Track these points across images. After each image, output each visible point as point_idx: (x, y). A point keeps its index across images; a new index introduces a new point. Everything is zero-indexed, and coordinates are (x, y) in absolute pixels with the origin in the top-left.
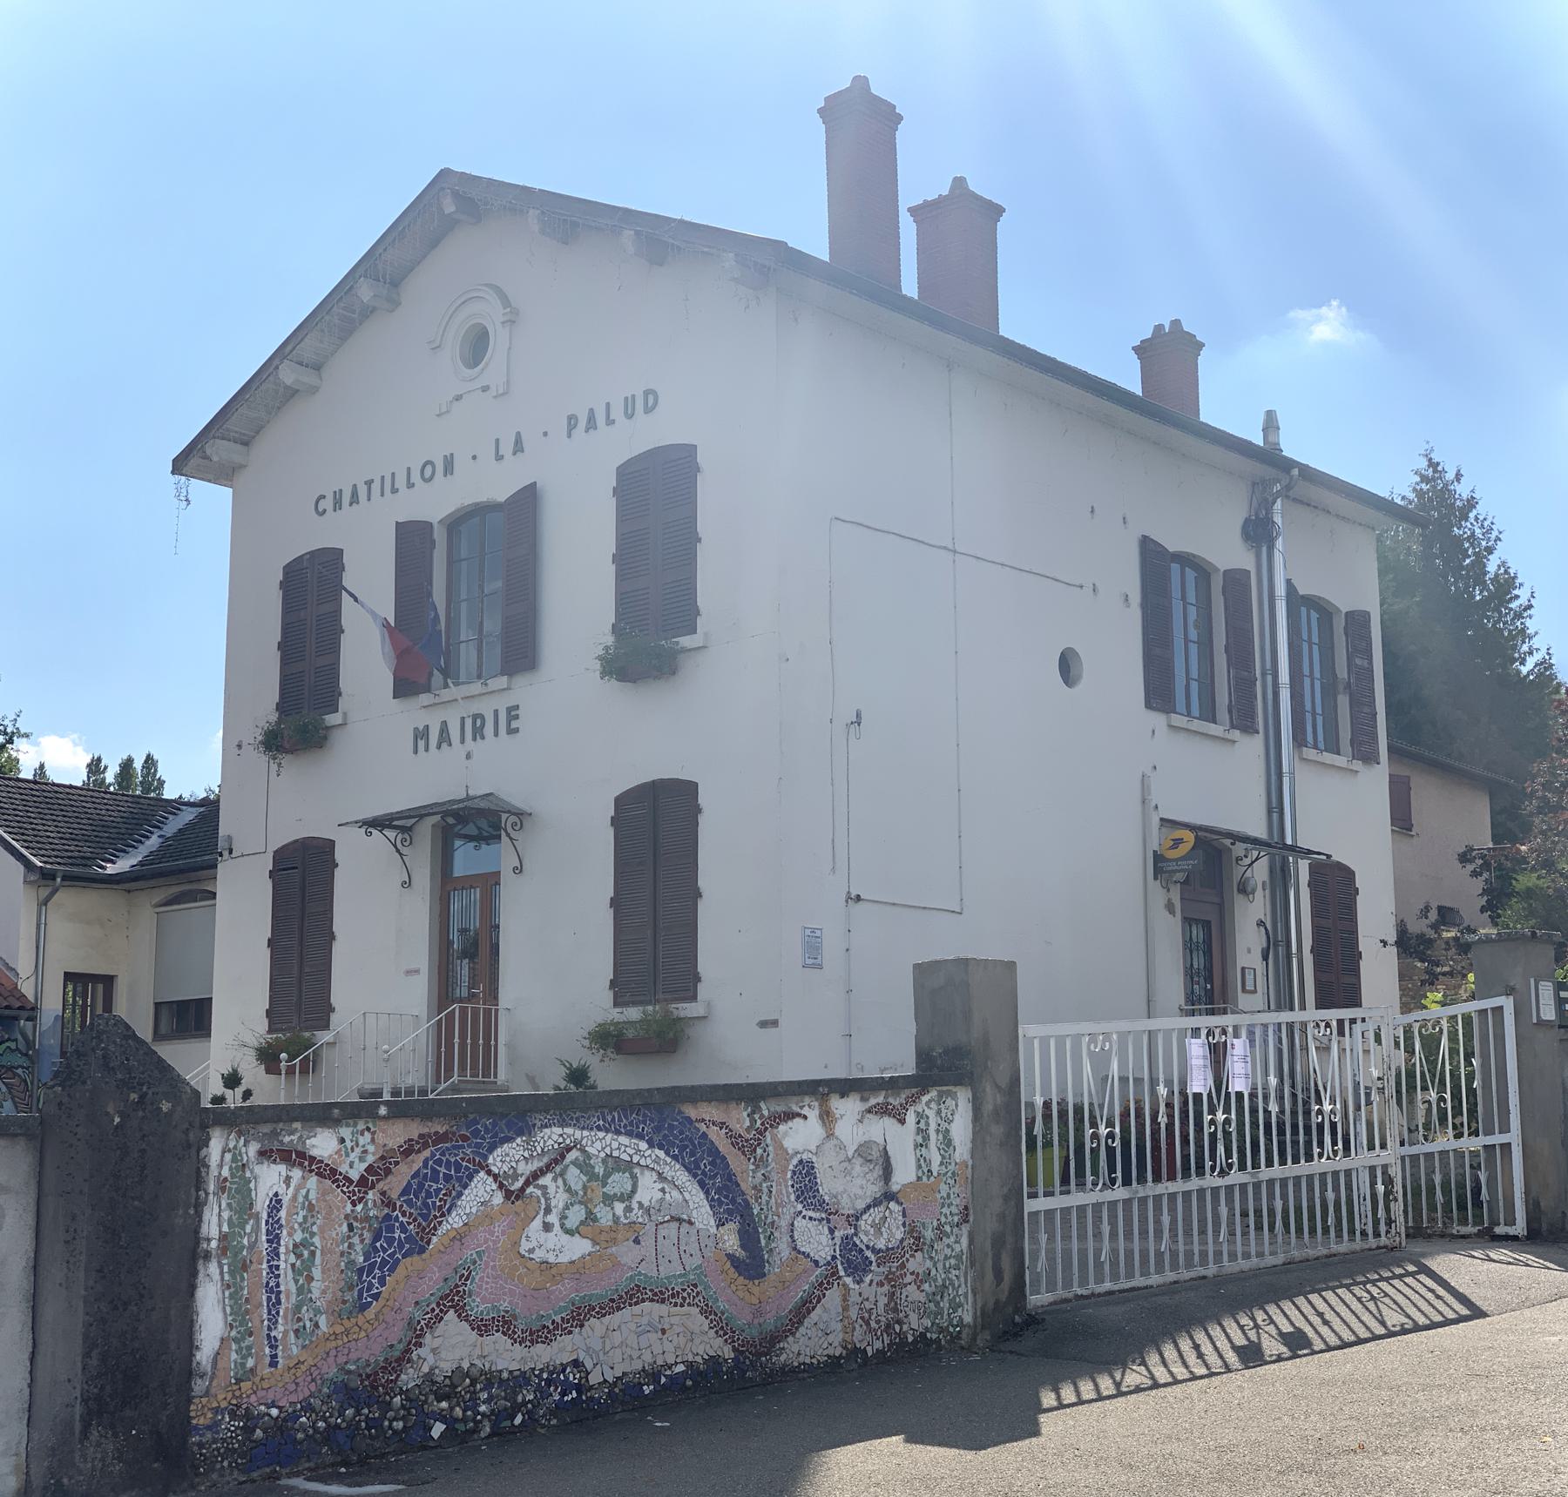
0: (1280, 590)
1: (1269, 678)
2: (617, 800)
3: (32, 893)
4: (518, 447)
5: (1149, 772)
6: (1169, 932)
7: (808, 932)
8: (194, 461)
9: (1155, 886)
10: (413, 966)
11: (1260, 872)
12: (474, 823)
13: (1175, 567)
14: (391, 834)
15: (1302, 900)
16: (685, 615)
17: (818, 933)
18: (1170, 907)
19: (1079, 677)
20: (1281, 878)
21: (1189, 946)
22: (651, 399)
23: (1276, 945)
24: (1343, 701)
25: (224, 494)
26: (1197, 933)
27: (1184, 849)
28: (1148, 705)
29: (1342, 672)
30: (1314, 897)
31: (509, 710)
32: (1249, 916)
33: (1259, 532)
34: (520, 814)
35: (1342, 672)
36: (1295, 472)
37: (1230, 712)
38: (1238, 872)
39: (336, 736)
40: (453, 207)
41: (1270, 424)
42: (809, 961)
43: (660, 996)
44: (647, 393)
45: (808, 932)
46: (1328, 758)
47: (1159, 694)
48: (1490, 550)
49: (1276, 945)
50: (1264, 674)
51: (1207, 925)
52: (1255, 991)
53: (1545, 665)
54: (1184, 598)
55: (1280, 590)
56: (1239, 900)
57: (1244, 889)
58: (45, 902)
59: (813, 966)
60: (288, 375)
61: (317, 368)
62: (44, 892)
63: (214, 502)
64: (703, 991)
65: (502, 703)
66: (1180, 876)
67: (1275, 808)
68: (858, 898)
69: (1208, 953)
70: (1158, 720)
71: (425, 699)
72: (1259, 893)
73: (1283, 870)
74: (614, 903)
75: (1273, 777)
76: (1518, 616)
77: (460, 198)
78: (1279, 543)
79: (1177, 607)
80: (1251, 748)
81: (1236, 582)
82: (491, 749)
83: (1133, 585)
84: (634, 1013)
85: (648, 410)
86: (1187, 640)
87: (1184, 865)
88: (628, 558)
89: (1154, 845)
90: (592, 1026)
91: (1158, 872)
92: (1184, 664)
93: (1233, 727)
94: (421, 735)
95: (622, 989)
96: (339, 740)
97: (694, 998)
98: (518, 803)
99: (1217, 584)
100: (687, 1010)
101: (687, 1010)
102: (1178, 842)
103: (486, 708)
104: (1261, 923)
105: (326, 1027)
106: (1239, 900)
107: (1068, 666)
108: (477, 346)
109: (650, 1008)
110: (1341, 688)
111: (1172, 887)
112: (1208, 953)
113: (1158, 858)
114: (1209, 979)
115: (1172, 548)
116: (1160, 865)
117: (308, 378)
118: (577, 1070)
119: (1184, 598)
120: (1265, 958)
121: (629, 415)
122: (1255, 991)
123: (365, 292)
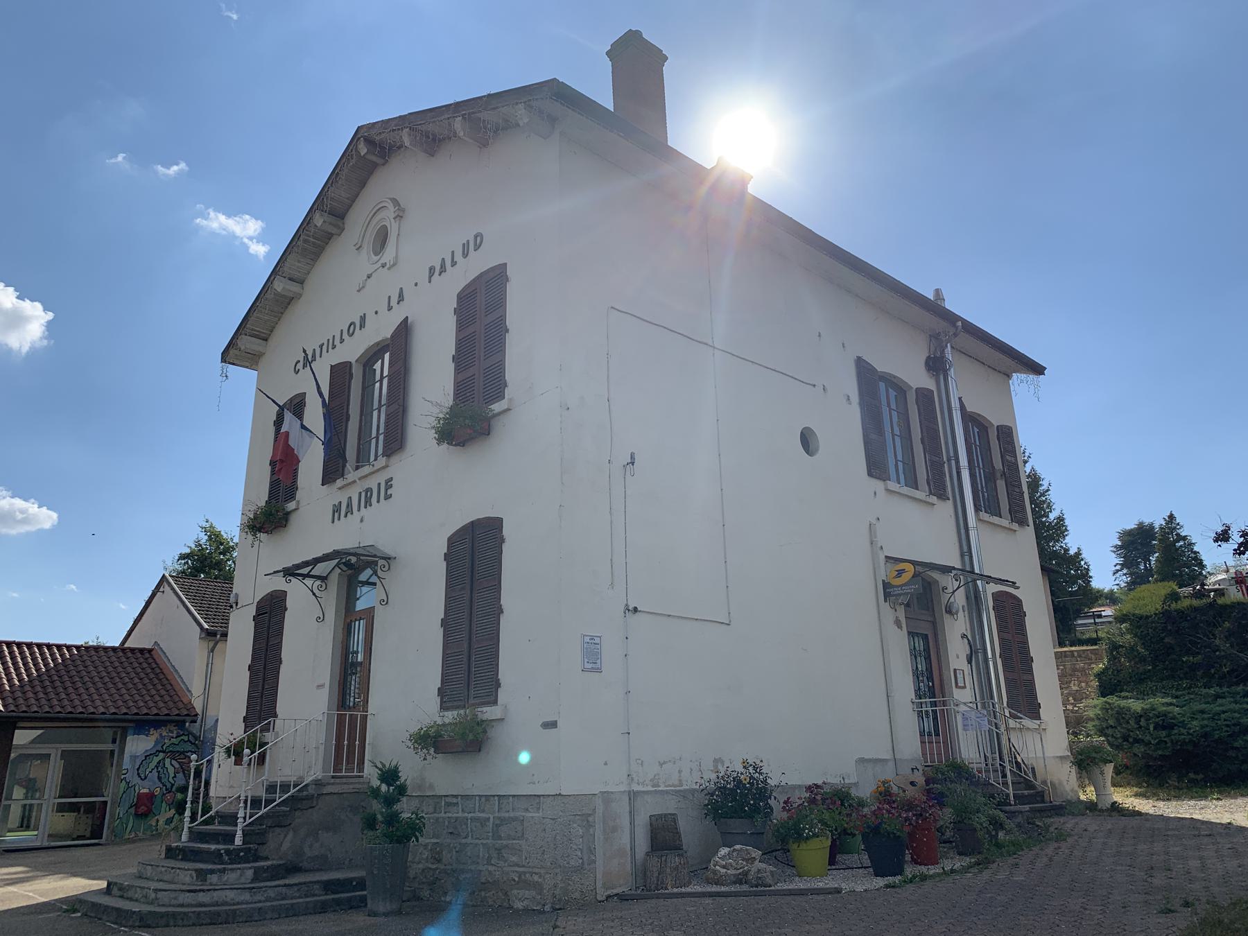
0: (955, 404)
1: (953, 462)
2: (449, 539)
3: (205, 644)
4: (401, 298)
5: (874, 522)
6: (899, 643)
7: (587, 639)
8: (232, 352)
9: (886, 607)
10: (321, 682)
11: (960, 599)
12: (355, 568)
13: (882, 385)
14: (309, 582)
15: (990, 619)
16: (496, 386)
17: (597, 640)
18: (898, 623)
19: (817, 450)
20: (975, 600)
21: (914, 653)
22: (478, 241)
23: (975, 653)
24: (1001, 484)
25: (252, 375)
26: (920, 644)
27: (906, 577)
28: (870, 474)
29: (998, 464)
30: (998, 617)
31: (387, 482)
32: (956, 630)
33: (936, 365)
34: (388, 559)
35: (998, 464)
36: (959, 324)
37: (928, 483)
38: (945, 598)
39: (294, 518)
40: (372, 151)
41: (938, 292)
42: (590, 666)
43: (472, 701)
44: (476, 237)
45: (587, 639)
46: (996, 520)
47: (876, 468)
48: (1025, 462)
49: (976, 653)
50: (949, 460)
51: (925, 637)
52: (965, 687)
53: (1061, 519)
54: (889, 405)
55: (955, 404)
56: (947, 619)
57: (949, 611)
58: (212, 651)
59: (592, 670)
60: (279, 286)
61: (301, 282)
62: (211, 644)
63: (245, 379)
64: (502, 695)
65: (381, 478)
66: (905, 599)
67: (966, 551)
68: (635, 610)
69: (928, 658)
70: (878, 485)
71: (340, 483)
72: (961, 614)
73: (976, 597)
74: (444, 623)
75: (963, 531)
76: (1043, 495)
77: (369, 142)
78: (952, 372)
79: (885, 409)
80: (945, 509)
81: (924, 397)
82: (378, 510)
83: (851, 387)
84: (450, 716)
85: (477, 248)
86: (893, 435)
87: (907, 590)
88: (463, 357)
89: (882, 575)
90: (414, 728)
91: (887, 596)
92: (893, 453)
93: (931, 493)
94: (337, 509)
95: (447, 697)
96: (295, 519)
97: (495, 702)
98: (389, 551)
99: (911, 398)
100: (489, 713)
101: (489, 713)
102: (900, 573)
103: (372, 483)
104: (964, 636)
105: (1099, 676)
106: (947, 619)
107: (807, 441)
108: (382, 239)
109: (462, 712)
110: (998, 475)
111: (898, 607)
112: (928, 658)
113: (886, 585)
114: (931, 678)
115: (880, 368)
116: (888, 590)
117: (295, 288)
118: (389, 770)
119: (889, 405)
120: (970, 662)
121: (465, 255)
122: (965, 687)
123: (318, 220)
